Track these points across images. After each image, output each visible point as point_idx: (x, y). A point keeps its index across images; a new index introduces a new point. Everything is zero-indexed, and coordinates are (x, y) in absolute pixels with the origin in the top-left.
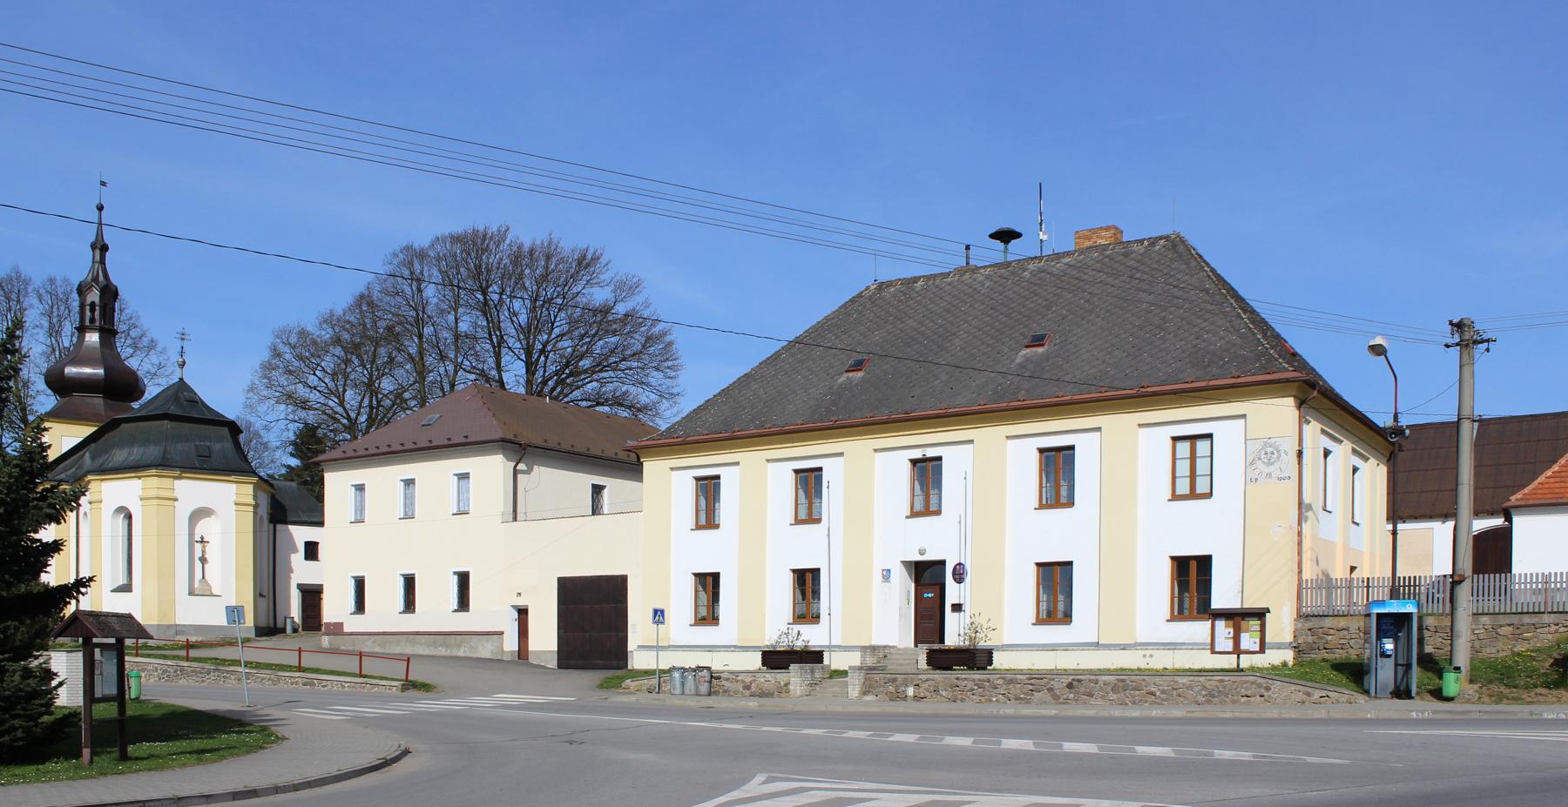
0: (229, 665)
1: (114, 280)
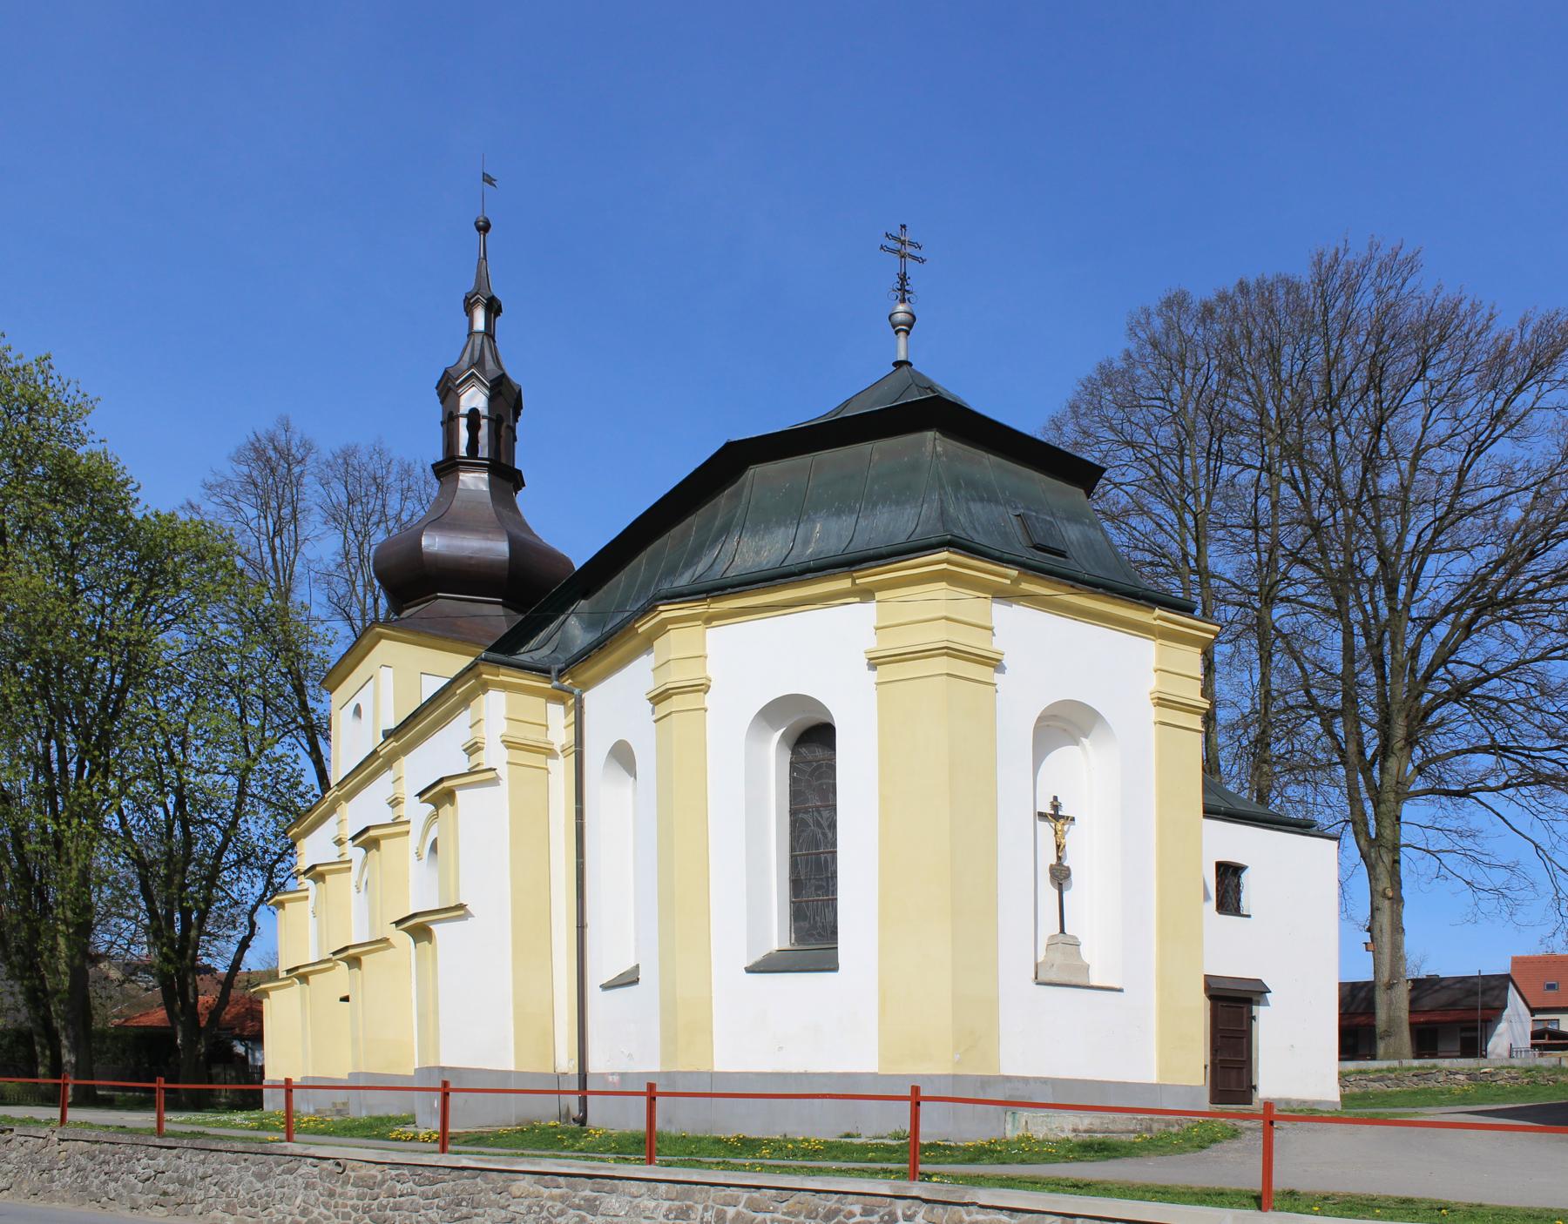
1: (515, 376)
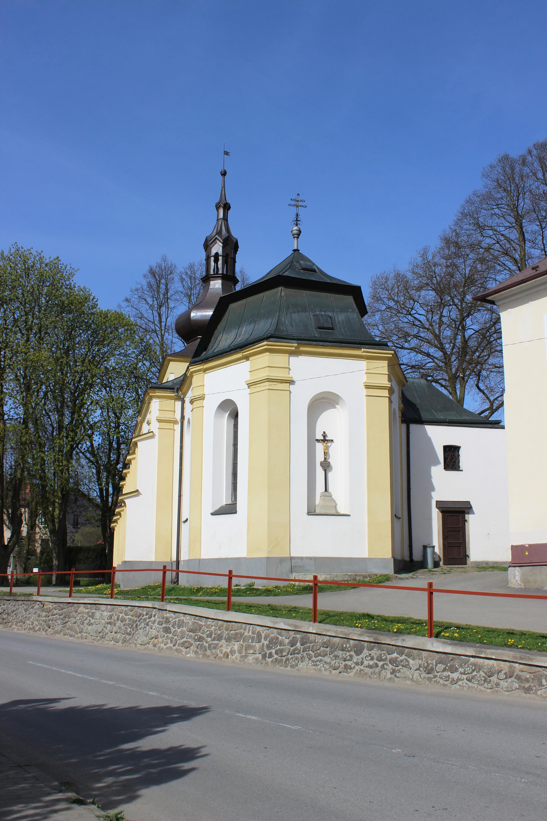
0: (399, 632)
1: (235, 234)
